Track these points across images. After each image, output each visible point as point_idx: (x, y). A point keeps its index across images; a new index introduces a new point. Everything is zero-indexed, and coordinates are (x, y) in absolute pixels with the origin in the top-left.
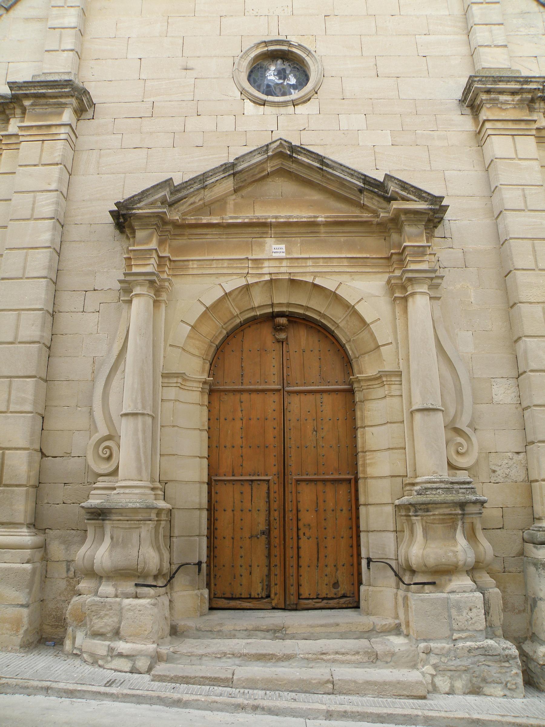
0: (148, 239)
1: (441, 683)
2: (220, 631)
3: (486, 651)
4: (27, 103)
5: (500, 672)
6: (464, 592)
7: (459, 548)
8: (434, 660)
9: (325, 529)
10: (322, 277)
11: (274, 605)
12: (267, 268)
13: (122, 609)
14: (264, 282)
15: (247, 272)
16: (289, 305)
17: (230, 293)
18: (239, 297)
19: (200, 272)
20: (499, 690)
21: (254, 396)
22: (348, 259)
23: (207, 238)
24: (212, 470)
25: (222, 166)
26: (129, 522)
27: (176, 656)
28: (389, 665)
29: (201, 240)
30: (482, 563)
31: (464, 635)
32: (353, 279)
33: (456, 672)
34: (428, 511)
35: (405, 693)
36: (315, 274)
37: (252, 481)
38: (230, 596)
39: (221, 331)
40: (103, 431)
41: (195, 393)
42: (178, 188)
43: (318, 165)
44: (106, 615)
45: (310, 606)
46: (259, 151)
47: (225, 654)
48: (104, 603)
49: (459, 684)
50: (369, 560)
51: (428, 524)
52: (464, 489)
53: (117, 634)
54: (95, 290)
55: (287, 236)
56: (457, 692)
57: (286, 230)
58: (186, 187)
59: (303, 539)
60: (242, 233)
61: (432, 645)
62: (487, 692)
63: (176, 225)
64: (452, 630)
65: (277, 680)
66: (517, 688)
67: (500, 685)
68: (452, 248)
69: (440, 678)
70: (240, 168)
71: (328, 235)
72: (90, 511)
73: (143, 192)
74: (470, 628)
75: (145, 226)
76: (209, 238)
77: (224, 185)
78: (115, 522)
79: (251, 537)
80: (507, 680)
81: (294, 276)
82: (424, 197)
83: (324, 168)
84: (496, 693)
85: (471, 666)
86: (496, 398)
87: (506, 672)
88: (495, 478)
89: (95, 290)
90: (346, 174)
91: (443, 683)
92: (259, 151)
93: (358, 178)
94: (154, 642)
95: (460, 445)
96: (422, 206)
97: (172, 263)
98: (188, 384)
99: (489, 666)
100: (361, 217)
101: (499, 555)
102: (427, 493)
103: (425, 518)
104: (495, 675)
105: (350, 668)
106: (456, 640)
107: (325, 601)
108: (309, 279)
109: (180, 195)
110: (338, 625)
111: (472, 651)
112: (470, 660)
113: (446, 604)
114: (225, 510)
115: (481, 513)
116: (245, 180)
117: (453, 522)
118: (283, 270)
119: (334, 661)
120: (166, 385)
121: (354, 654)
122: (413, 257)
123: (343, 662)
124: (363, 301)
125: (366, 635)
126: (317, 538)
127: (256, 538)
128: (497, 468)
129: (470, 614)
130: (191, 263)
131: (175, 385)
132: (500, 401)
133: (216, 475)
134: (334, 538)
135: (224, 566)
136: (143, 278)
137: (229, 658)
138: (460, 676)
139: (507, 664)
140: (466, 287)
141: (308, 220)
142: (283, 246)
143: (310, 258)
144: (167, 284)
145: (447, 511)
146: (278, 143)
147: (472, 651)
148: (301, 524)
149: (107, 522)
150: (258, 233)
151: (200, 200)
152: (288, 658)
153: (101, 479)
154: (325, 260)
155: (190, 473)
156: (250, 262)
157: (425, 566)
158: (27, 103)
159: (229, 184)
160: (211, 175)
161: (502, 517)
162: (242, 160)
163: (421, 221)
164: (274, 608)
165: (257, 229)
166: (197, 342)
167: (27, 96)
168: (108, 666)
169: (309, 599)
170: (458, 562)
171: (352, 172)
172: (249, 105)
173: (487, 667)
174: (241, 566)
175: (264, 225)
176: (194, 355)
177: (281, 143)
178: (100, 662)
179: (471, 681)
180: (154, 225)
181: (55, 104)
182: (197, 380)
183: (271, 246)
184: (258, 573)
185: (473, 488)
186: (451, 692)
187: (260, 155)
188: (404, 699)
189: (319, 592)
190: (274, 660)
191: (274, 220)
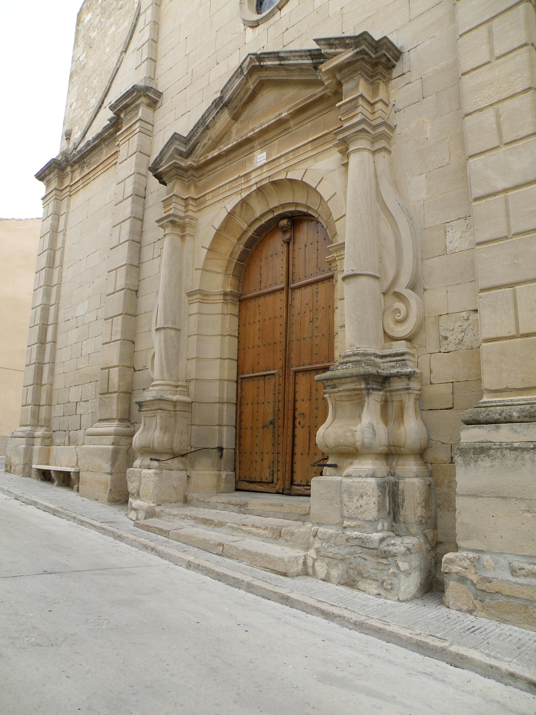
1: (320, 568)
2: (209, 502)
3: (363, 542)
5: (376, 569)
6: (360, 476)
7: (359, 427)
8: (317, 544)
9: (316, 417)
12: (254, 179)
13: (141, 476)
18: (244, 212)
20: (373, 588)
22: (312, 143)
24: (240, 370)
25: (212, 103)
27: (162, 514)
28: (288, 543)
30: (404, 447)
31: (353, 523)
32: (316, 161)
33: (333, 560)
34: (335, 387)
35: (270, 566)
36: (287, 170)
37: (265, 376)
38: (249, 480)
41: (218, 305)
42: (188, 137)
43: (277, 63)
44: (134, 480)
45: (300, 492)
46: (236, 75)
49: (335, 573)
51: (338, 402)
52: (394, 361)
54: (159, 240)
56: (332, 580)
57: (266, 137)
58: (194, 134)
59: (298, 427)
60: (238, 155)
61: (322, 529)
62: (362, 588)
63: (199, 168)
64: (342, 516)
65: (191, 537)
66: (391, 589)
67: (376, 583)
68: (410, 83)
69: (320, 564)
70: (226, 99)
71: (298, 127)
73: (161, 153)
74: (359, 517)
77: (222, 119)
80: (384, 578)
81: (273, 178)
84: (369, 590)
85: (347, 556)
86: (450, 247)
87: (384, 570)
88: (446, 346)
89: (159, 240)
91: (321, 568)
92: (236, 75)
94: (153, 502)
95: (398, 311)
96: (347, 55)
97: (197, 201)
98: (211, 298)
99: (365, 559)
100: (315, 95)
101: (445, 442)
102: (338, 368)
103: (332, 395)
104: (371, 570)
105: (258, 540)
106: (345, 528)
109: (191, 143)
110: (282, 505)
111: (350, 540)
112: (347, 550)
113: (339, 488)
115: (408, 389)
116: (236, 106)
117: (360, 398)
118: (264, 176)
119: (249, 533)
120: (191, 302)
121: (264, 529)
122: (346, 115)
123: (255, 535)
125: (303, 518)
126: (309, 427)
128: (448, 334)
129: (361, 502)
131: (196, 301)
132: (456, 249)
133: (243, 374)
137: (189, 519)
138: (336, 565)
139: (385, 561)
140: (421, 123)
141: (275, 120)
143: (282, 156)
144: (187, 220)
145: (352, 386)
146: (248, 59)
147: (350, 540)
148: (297, 413)
150: (248, 150)
151: (208, 141)
152: (220, 524)
154: (294, 152)
157: (326, 446)
159: (225, 116)
160: (208, 116)
161: (453, 393)
162: (226, 90)
163: (356, 71)
165: (247, 147)
166: (220, 261)
169: (300, 485)
170: (355, 443)
173: (363, 560)
175: (249, 141)
176: (218, 273)
177: (251, 58)
179: (347, 572)
180: (174, 176)
185: (404, 360)
186: (326, 579)
187: (238, 79)
188: (269, 571)
190: (213, 526)
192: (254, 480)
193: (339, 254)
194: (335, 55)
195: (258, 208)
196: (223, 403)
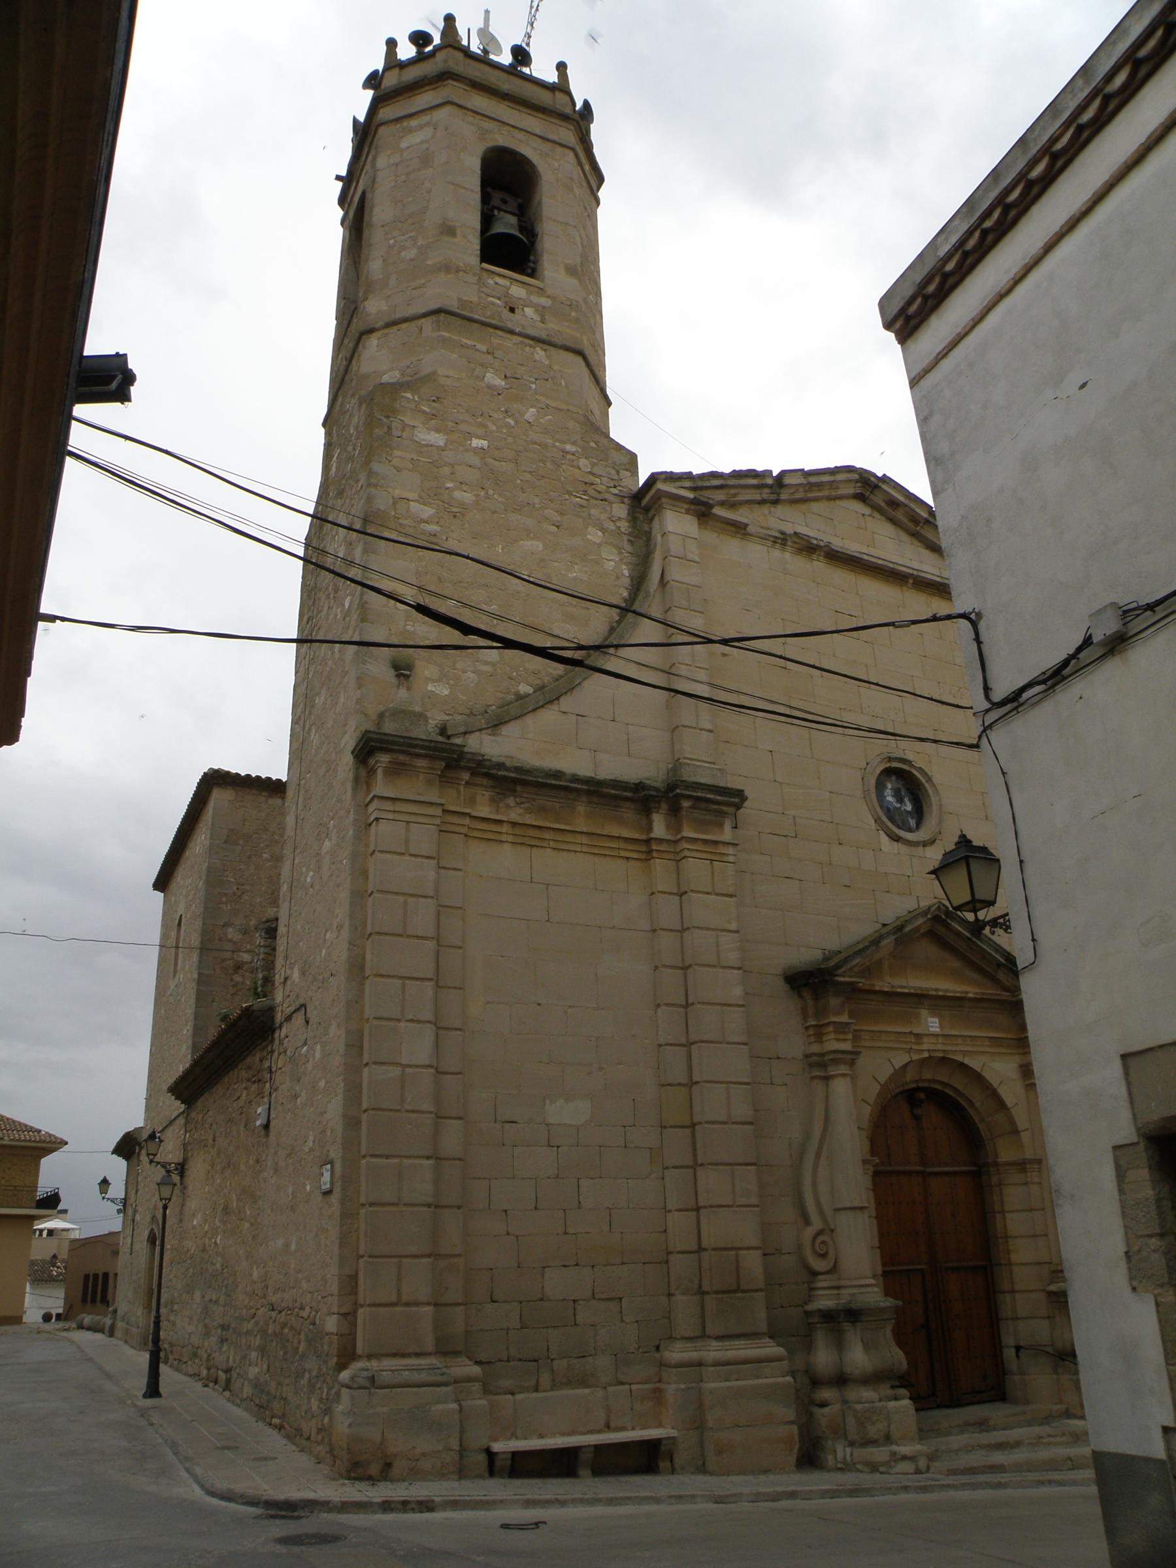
4: (686, 804)
16: (933, 1081)
36: (965, 1053)
37: (908, 1270)
40: (817, 1224)
47: (973, 1447)
50: (1018, 1348)
53: (888, 1439)
93: (1002, 955)
108: (959, 1058)
118: (940, 1047)
119: (1050, 1444)
142: (937, 1020)
152: (1018, 1444)
153: (820, 1277)
158: (686, 804)
167: (689, 797)
168: (893, 1471)
172: (884, 839)
178: (881, 1469)
181: (715, 811)
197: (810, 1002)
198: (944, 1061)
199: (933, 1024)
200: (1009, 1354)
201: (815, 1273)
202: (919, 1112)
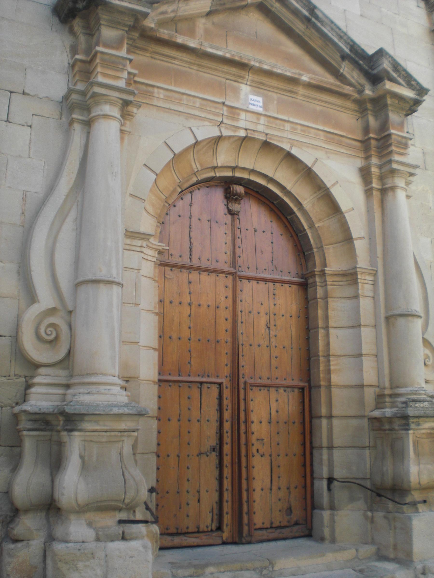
0: (118, 45)
10: (299, 147)
11: (224, 539)
12: (244, 121)
14: (237, 138)
15: (221, 120)
16: (253, 171)
17: (201, 142)
19: (167, 105)
21: (204, 276)
23: (174, 64)
26: (108, 434)
29: (166, 64)
36: (293, 143)
37: (201, 383)
38: (175, 531)
39: (176, 188)
43: (306, 13)
48: (82, 551)
55: (263, 87)
60: (216, 70)
72: (33, 417)
75: (114, 24)
76: (176, 65)
78: (88, 434)
79: (200, 454)
82: (412, 85)
83: (313, 19)
89: (24, 93)
90: (334, 34)
93: (346, 43)
107: (278, 531)
108: (286, 147)
114: (169, 420)
118: (261, 128)
124: (338, 185)
127: (205, 455)
130: (156, 90)
131: (138, 249)
134: (287, 455)
135: (167, 493)
136: (117, 94)
142: (260, 99)
143: (288, 121)
149: (76, 433)
150: (234, 75)
155: (147, 367)
156: (225, 108)
163: (403, 109)
164: (224, 543)
165: (234, 70)
166: (153, 197)
171: (342, 34)
174: (188, 492)
175: (242, 66)
182: (154, 247)
183: (246, 95)
184: (209, 499)
189: (273, 520)
191: (257, 64)
192: (184, 530)
193: (363, 278)
194: (400, 84)
195: (224, 157)
196: (364, 448)
197: (82, 38)
198: (267, 146)
199: (256, 102)
200: (322, 485)
201: (37, 366)
202: (235, 207)
